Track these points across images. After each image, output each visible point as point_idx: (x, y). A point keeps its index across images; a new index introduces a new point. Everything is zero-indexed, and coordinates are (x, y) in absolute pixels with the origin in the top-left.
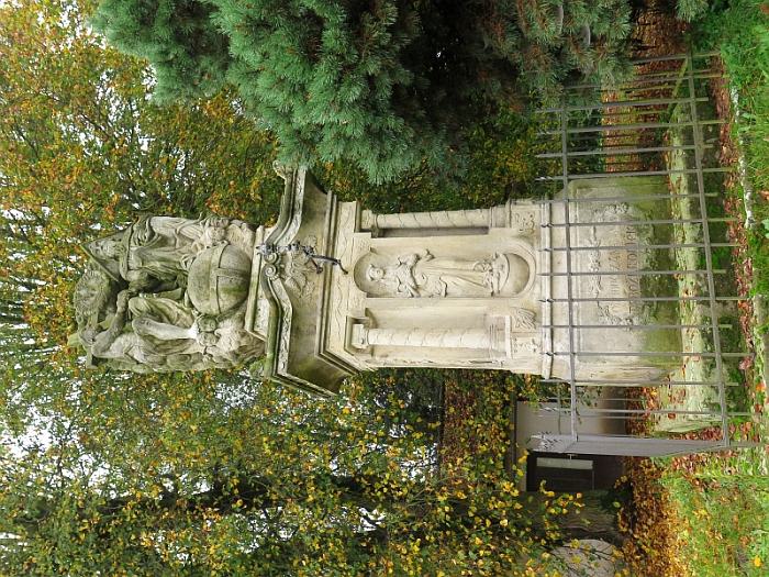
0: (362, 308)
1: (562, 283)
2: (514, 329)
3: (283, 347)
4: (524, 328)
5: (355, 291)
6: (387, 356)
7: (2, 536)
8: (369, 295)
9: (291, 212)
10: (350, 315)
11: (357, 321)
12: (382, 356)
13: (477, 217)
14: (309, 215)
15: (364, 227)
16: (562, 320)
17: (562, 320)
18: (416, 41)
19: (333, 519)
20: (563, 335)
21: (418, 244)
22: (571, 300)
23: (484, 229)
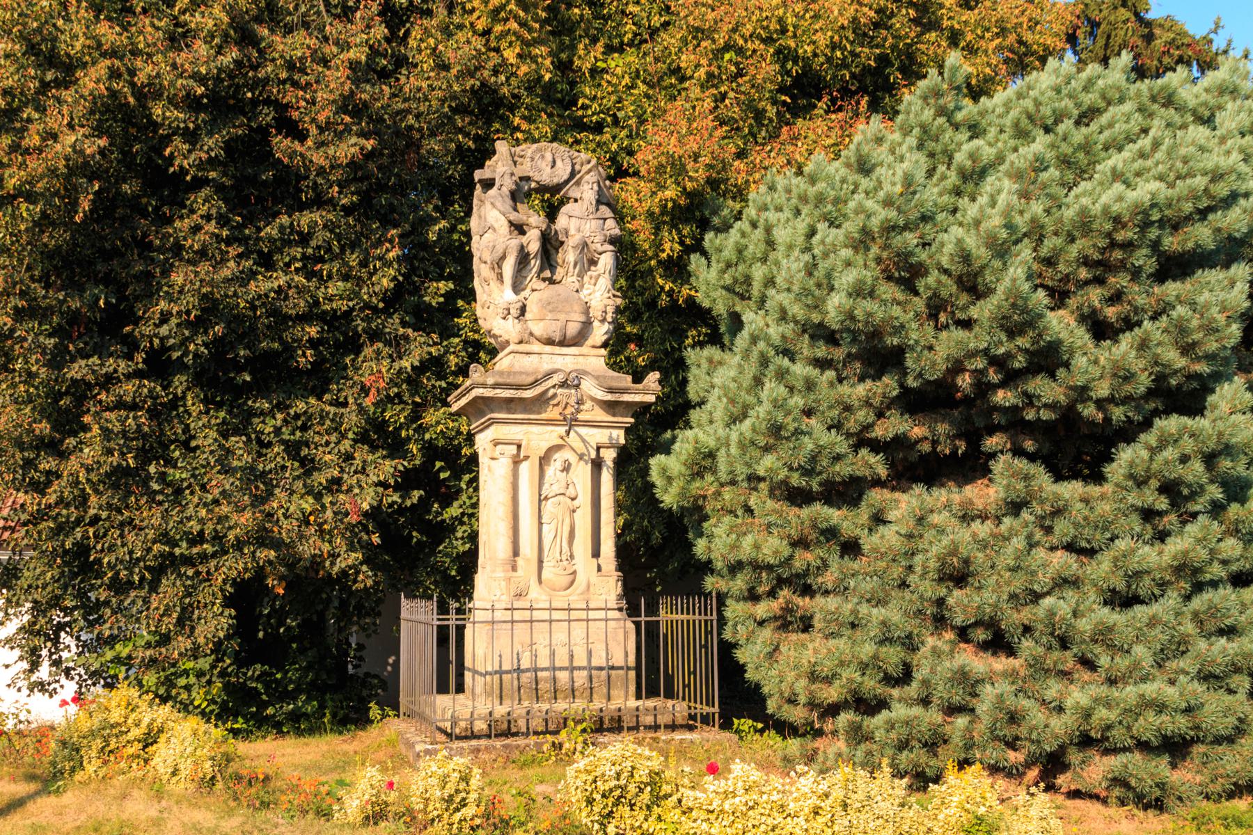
1: (545, 615)
3: (498, 391)
4: (513, 587)
5: (545, 446)
9: (611, 390)
11: (519, 447)
14: (610, 407)
16: (518, 615)
17: (518, 615)
20: (507, 616)
22: (588, 609)
23: (596, 554)
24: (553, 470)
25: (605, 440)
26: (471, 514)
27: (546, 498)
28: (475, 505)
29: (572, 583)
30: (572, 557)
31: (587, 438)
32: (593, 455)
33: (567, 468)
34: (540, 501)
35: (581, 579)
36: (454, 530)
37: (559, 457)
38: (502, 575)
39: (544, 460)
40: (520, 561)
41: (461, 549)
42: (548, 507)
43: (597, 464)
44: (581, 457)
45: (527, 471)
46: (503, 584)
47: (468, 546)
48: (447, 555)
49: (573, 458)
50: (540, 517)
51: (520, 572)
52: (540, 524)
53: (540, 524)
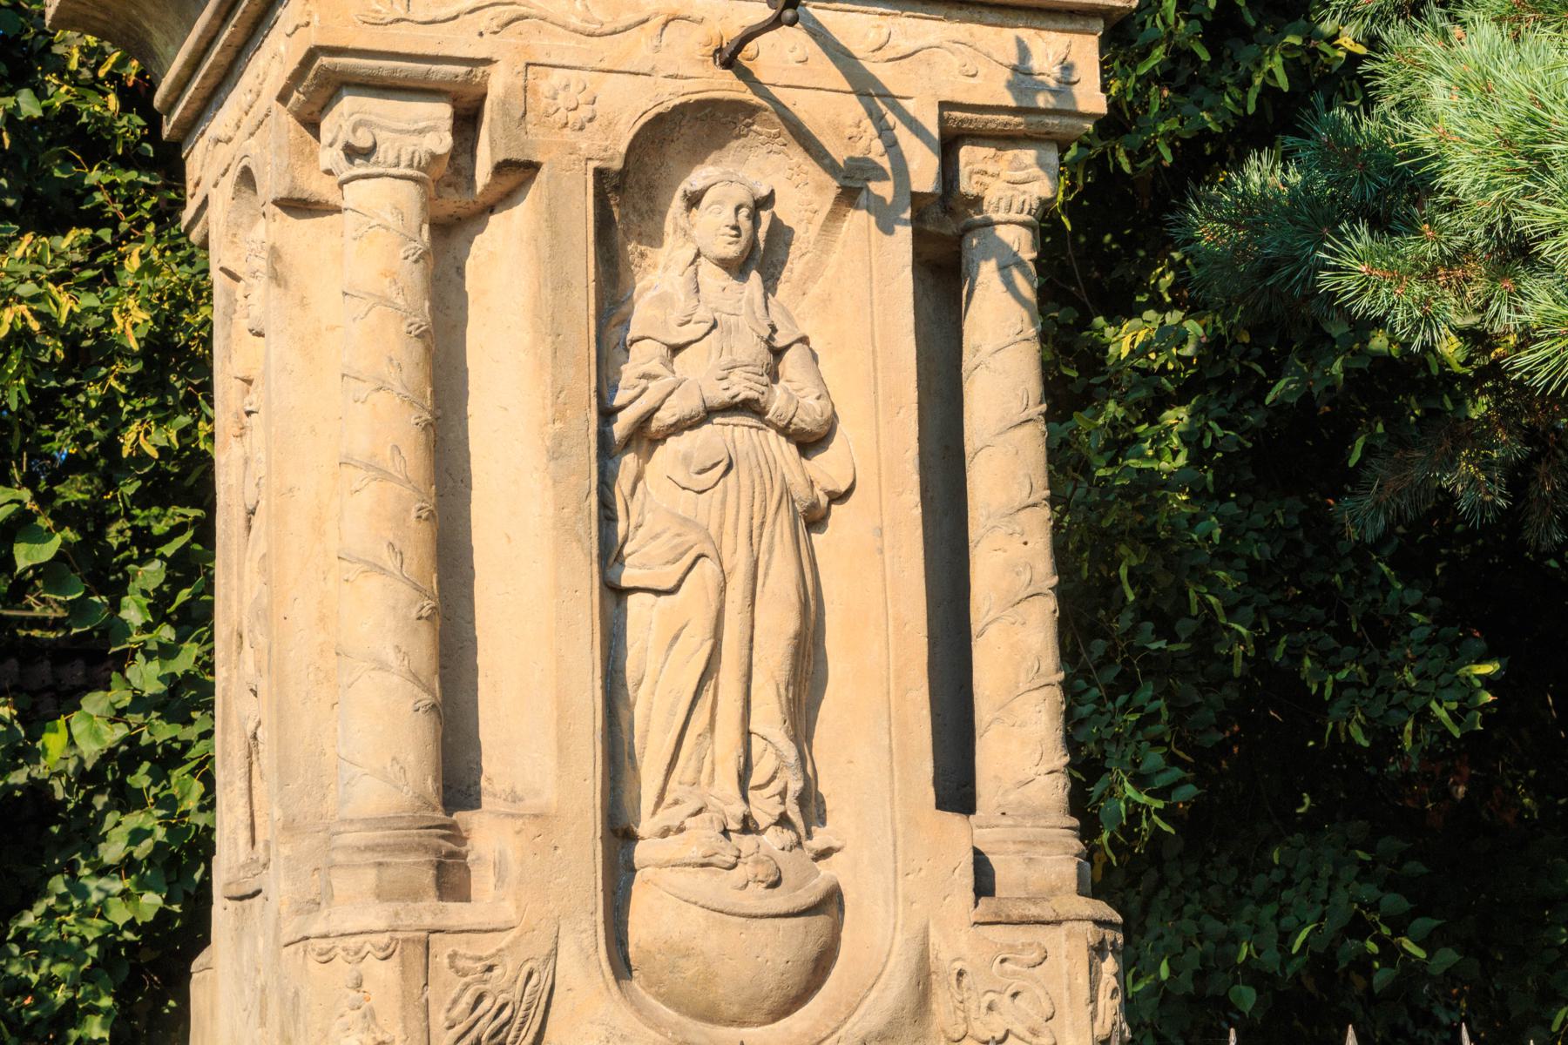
0: (539, 144)
2: (442, 948)
5: (626, 107)
6: (277, 278)
7: (2, 700)
8: (608, 185)
10: (498, 83)
11: (467, 121)
12: (275, 254)
13: (1023, 741)
15: (966, 153)
18: (80, 227)
19: (1118, 661)
21: (878, 445)
23: (956, 789)
24: (674, 274)
25: (993, 89)
26: (173, 741)
27: (645, 436)
28: (189, 696)
29: (822, 964)
30: (811, 804)
31: (884, 73)
32: (924, 172)
33: (761, 255)
34: (607, 451)
35: (874, 941)
36: (87, 834)
37: (724, 179)
38: (375, 916)
39: (627, 198)
40: (488, 835)
41: (120, 914)
42: (659, 489)
43: (944, 255)
44: (852, 183)
45: (518, 267)
46: (383, 975)
47: (151, 902)
48: (58, 951)
49: (801, 196)
50: (609, 553)
51: (489, 899)
52: (614, 594)
53: (614, 594)
